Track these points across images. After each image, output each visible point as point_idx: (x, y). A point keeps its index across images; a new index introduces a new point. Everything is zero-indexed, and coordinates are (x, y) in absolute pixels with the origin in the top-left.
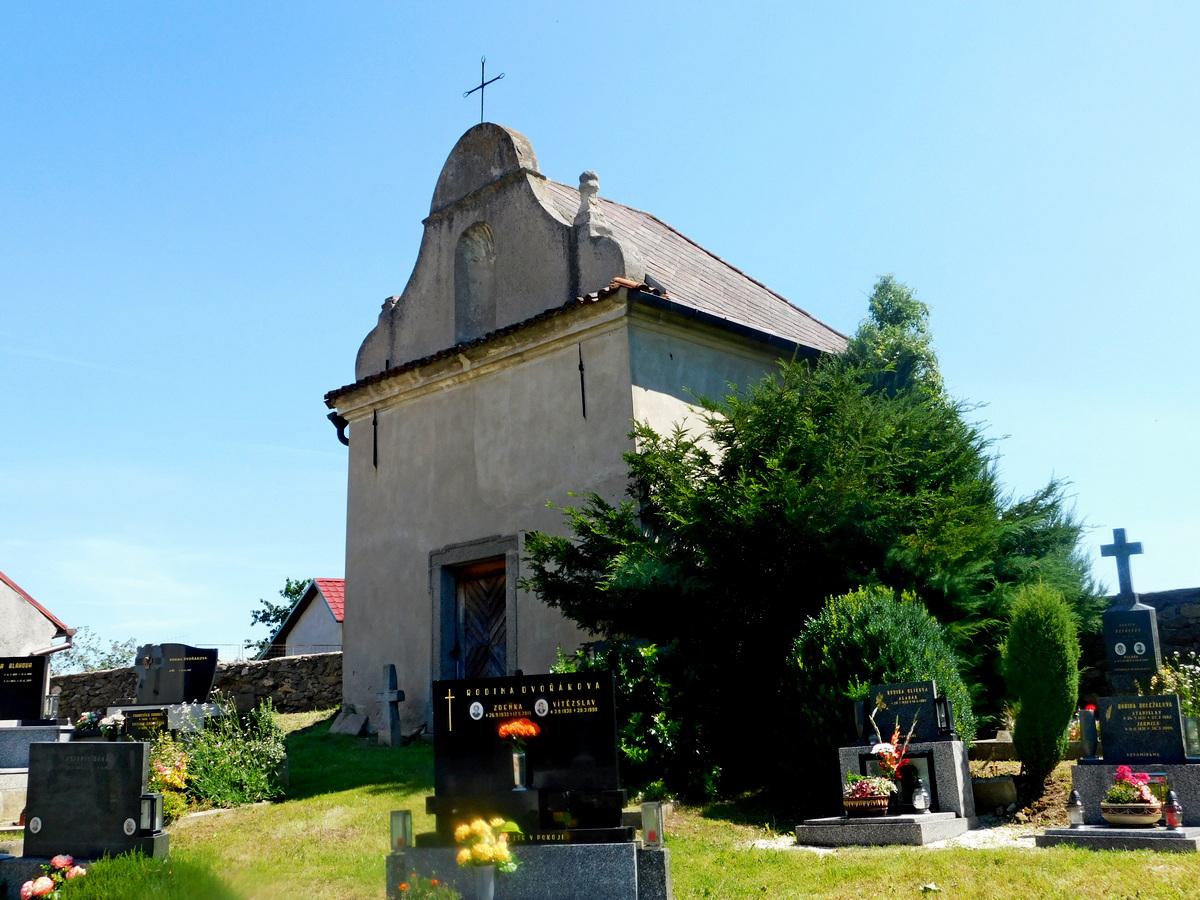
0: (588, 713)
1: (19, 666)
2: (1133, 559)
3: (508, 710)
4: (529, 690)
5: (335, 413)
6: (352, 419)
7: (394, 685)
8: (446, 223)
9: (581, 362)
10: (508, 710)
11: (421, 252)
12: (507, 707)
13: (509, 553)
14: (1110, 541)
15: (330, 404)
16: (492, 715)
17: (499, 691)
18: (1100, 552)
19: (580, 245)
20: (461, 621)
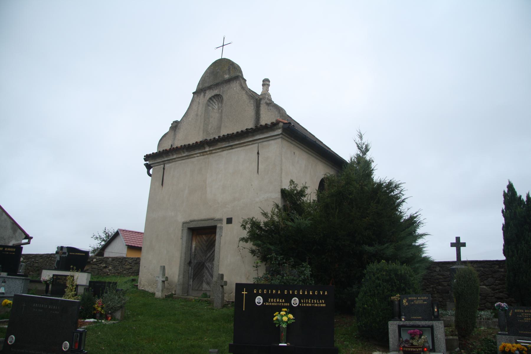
0: (320, 307)
1: (9, 249)
2: (462, 249)
3: (276, 302)
4: (289, 292)
5: (147, 163)
6: (154, 166)
7: (164, 274)
8: (202, 94)
9: (258, 151)
10: (276, 302)
11: (190, 104)
12: (276, 300)
13: (219, 225)
14: (454, 241)
15: (145, 160)
16: (267, 304)
17: (272, 292)
19: (261, 105)
20: (193, 251)
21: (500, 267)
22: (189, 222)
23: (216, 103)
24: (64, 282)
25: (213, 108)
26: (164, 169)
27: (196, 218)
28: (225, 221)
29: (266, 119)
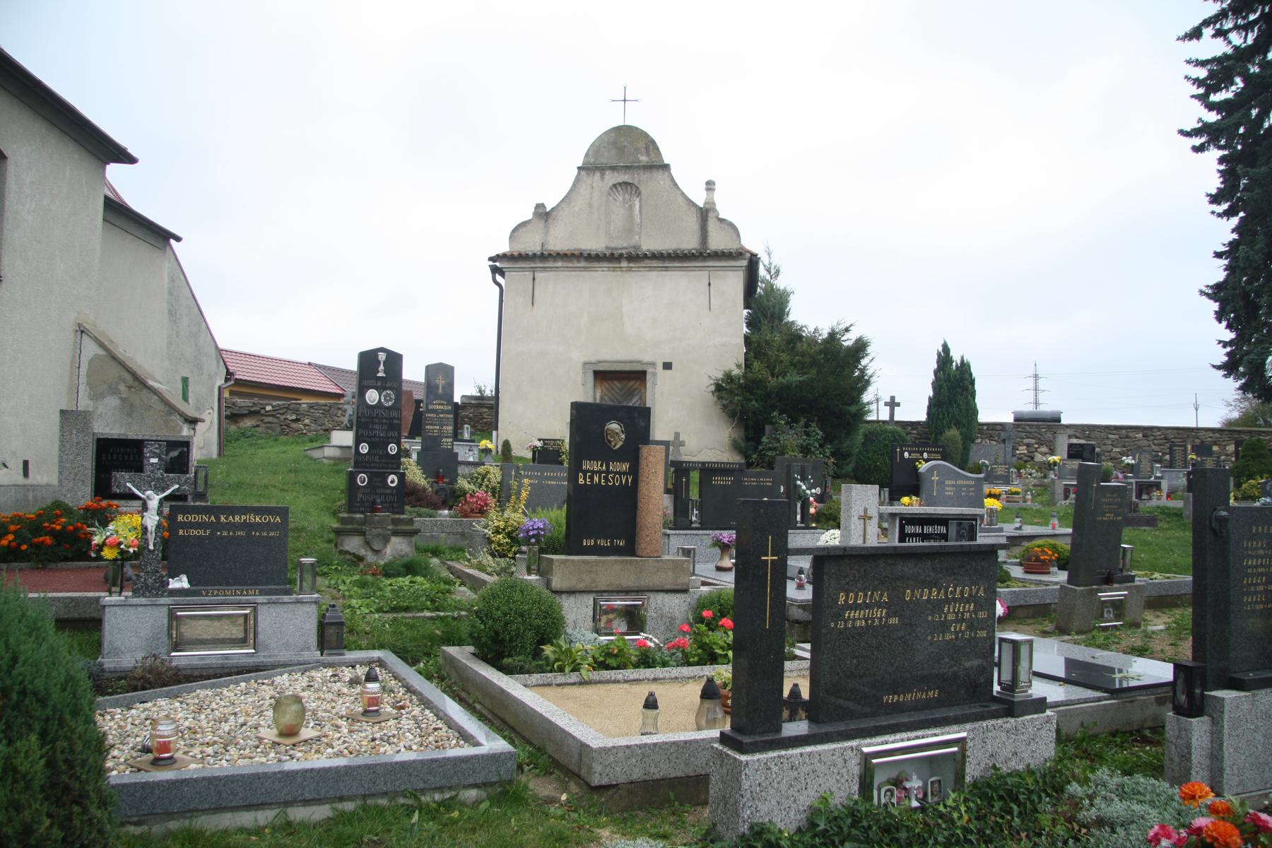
13: (650, 370)
18: (185, 375)
21: (913, 429)
27: (608, 358)
28: (660, 366)
29: (717, 242)
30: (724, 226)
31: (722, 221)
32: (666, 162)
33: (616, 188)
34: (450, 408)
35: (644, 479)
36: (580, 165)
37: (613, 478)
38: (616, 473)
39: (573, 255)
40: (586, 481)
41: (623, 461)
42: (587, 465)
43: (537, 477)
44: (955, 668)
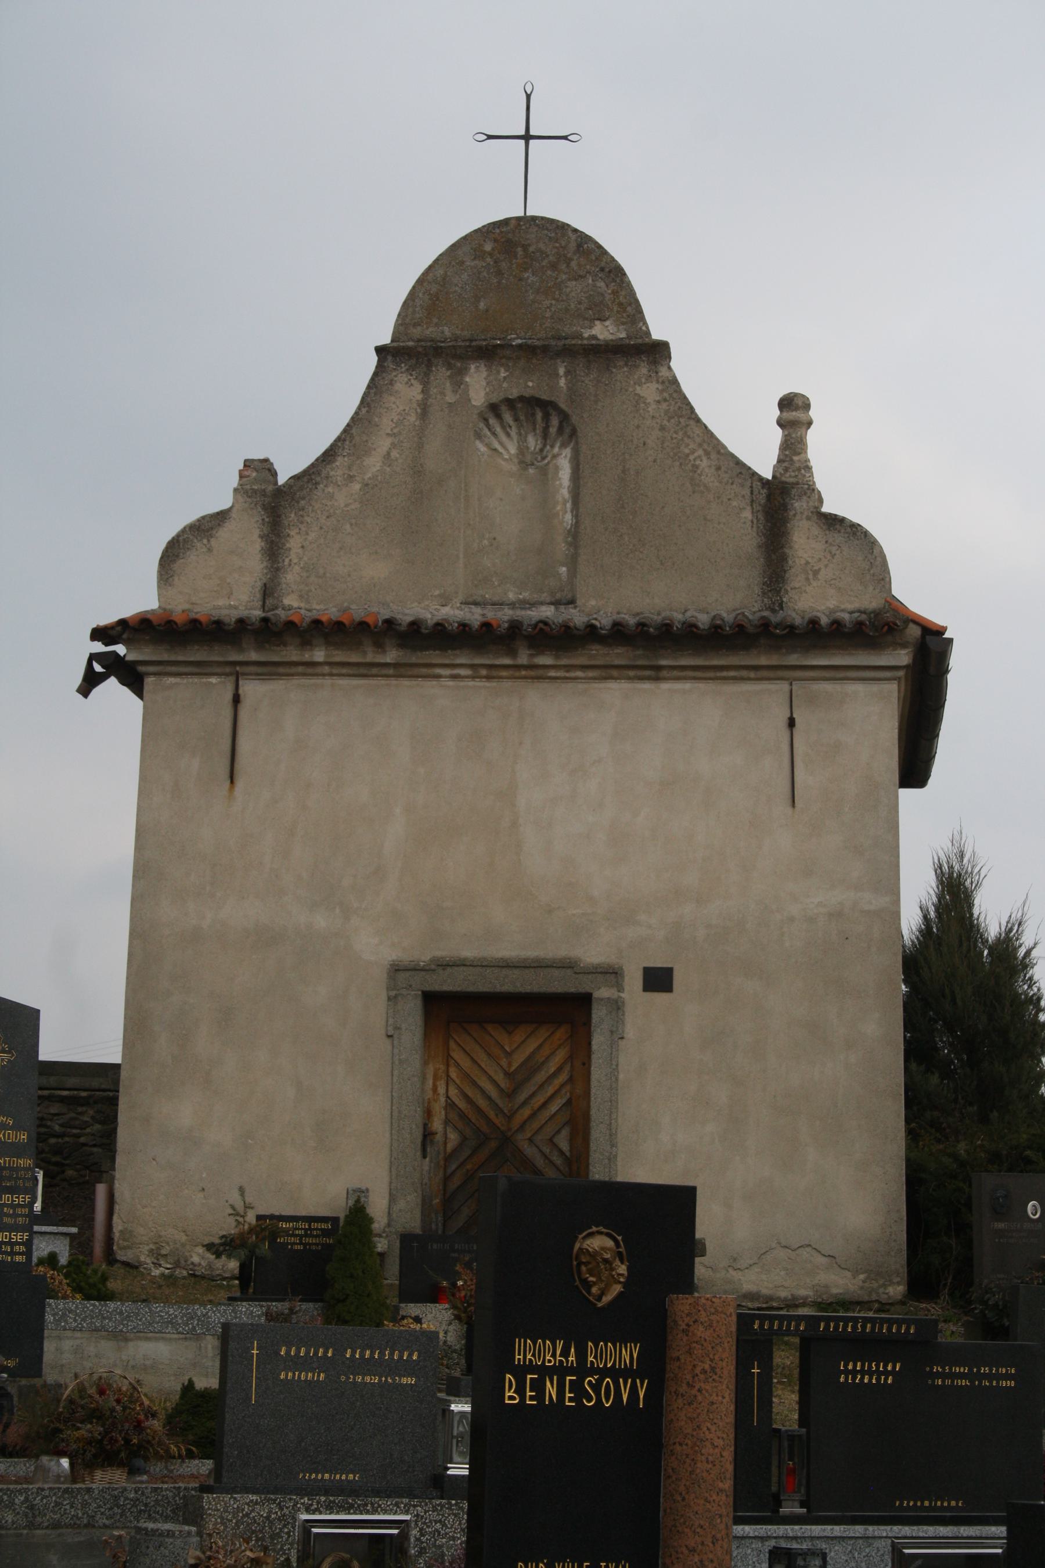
11: (365, 401)
13: (603, 993)
22: (433, 967)
23: (513, 432)
24: (305, 1245)
25: (495, 450)
26: (236, 700)
28: (634, 980)
30: (838, 538)
31: (834, 522)
32: (656, 335)
33: (499, 416)
34: (24, 1137)
35: (683, 1389)
36: (386, 339)
37: (596, 1388)
38: (604, 1372)
39: (363, 626)
40: (522, 1396)
41: (621, 1338)
42: (525, 1352)
43: (324, 1364)
44: (636, 377)
